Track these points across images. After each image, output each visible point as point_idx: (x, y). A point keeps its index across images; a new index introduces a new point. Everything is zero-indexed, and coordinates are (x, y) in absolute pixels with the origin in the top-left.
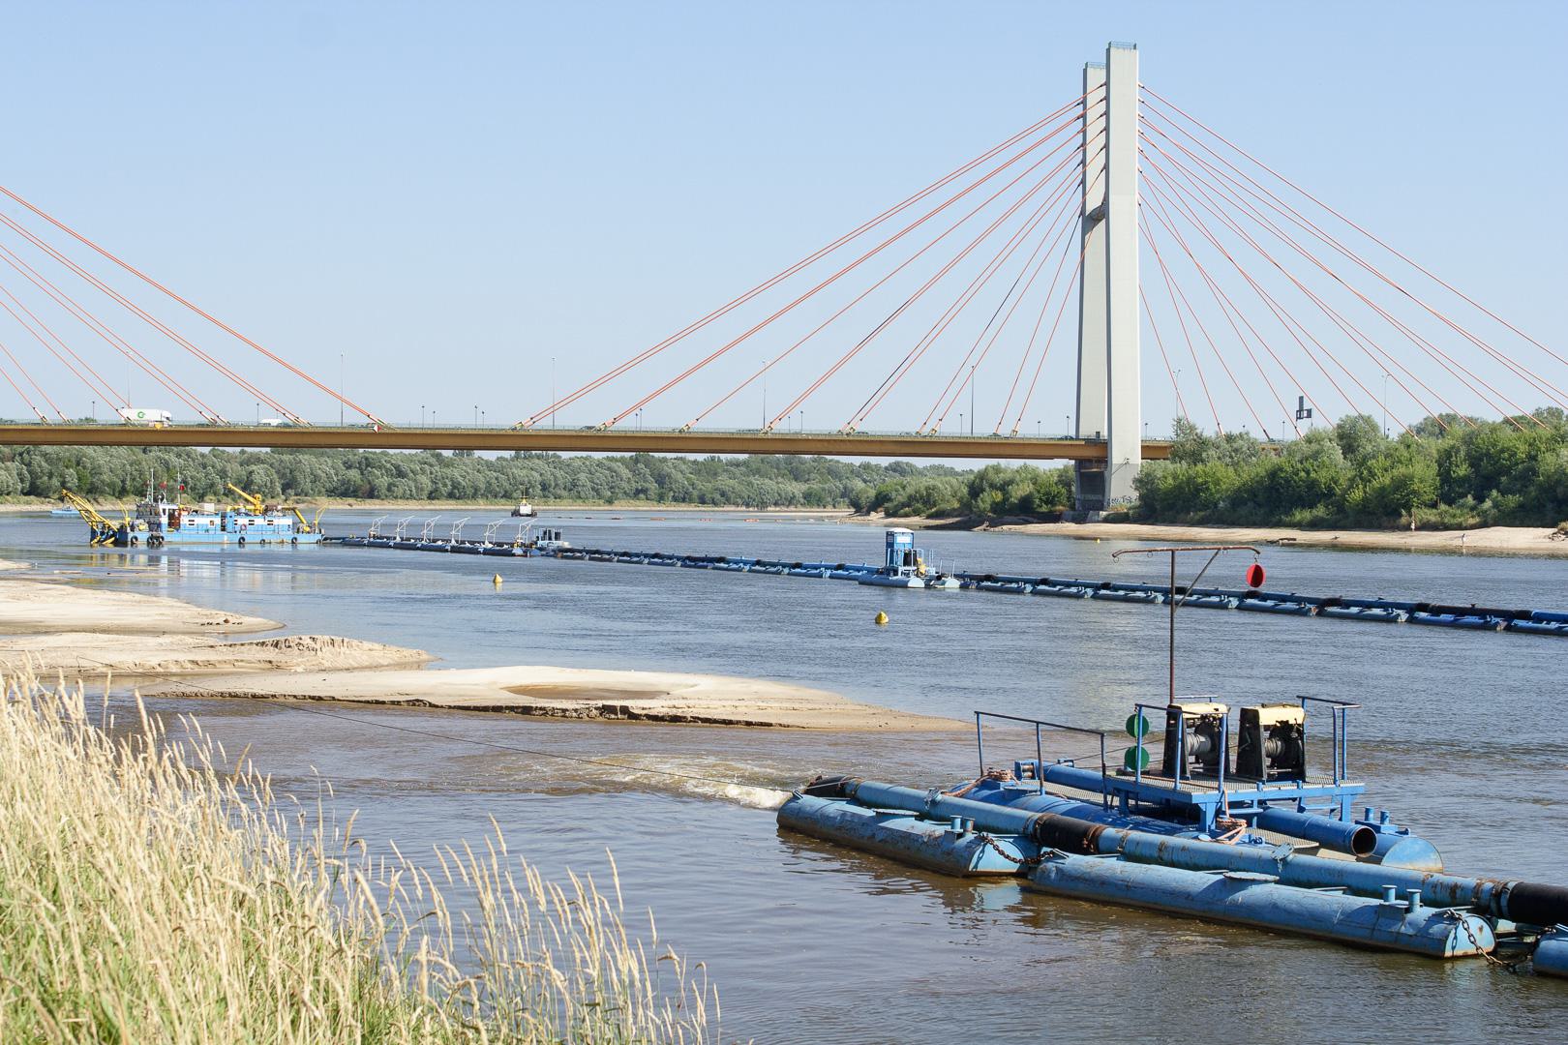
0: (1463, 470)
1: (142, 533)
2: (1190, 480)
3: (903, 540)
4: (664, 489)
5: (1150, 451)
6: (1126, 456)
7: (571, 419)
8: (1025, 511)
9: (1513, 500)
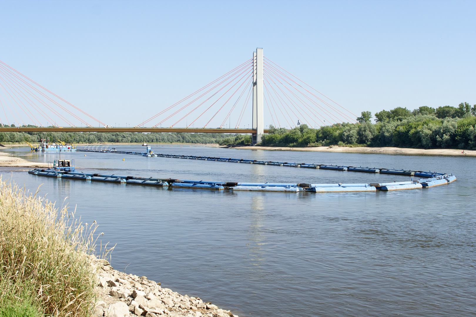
0: (321, 135)
1: (41, 149)
2: (272, 137)
3: (149, 148)
4: (184, 140)
5: (265, 131)
6: (260, 132)
7: (165, 126)
8: (242, 144)
9: (328, 141)
